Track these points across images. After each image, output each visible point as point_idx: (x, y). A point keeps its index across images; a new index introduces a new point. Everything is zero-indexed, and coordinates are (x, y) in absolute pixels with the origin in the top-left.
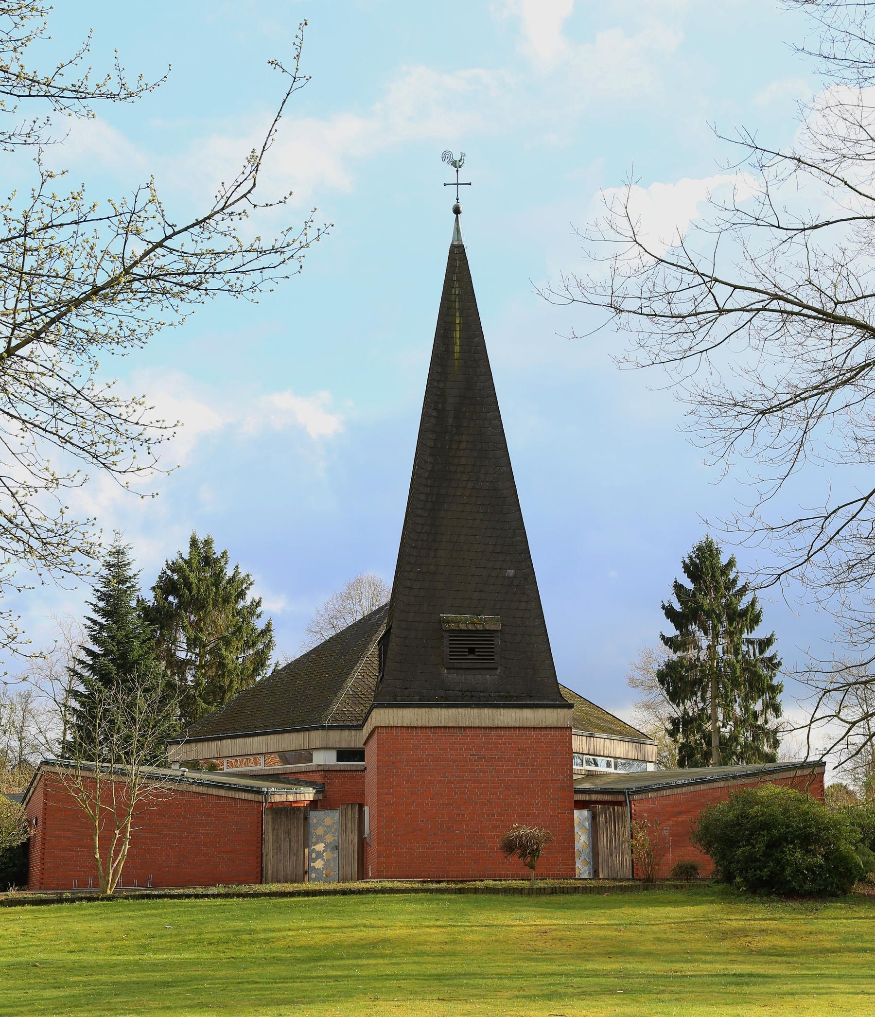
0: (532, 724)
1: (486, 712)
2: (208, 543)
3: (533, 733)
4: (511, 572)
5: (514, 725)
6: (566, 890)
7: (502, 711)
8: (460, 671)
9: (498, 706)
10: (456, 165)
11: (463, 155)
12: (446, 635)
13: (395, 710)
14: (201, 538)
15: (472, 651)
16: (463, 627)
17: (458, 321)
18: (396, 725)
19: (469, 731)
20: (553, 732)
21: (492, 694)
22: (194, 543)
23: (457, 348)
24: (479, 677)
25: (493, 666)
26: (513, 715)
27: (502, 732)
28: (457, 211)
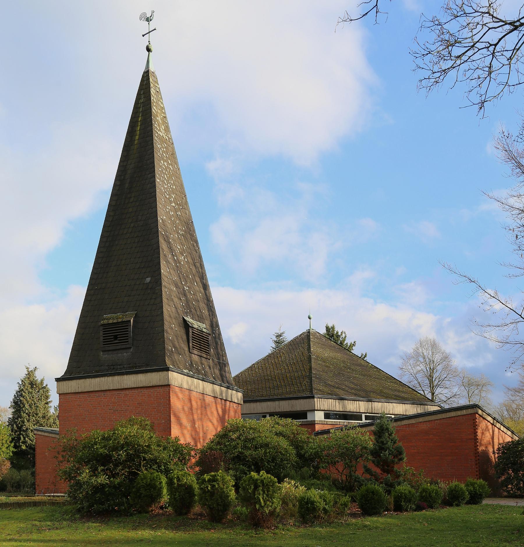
0: (145, 385)
1: (116, 378)
2: (333, 328)
3: (146, 391)
4: (148, 280)
5: (133, 386)
6: (32, 504)
7: (125, 377)
8: (110, 352)
9: (122, 374)
10: (148, 20)
11: (153, 12)
12: (101, 328)
13: (67, 382)
14: (330, 326)
15: (116, 337)
16: (111, 321)
17: (140, 120)
18: (67, 392)
19: (108, 393)
20: (158, 390)
21: (125, 366)
22: (327, 328)
23: (137, 137)
24: (120, 355)
25: (128, 346)
26: (133, 379)
27: (127, 392)
28: (149, 50)
